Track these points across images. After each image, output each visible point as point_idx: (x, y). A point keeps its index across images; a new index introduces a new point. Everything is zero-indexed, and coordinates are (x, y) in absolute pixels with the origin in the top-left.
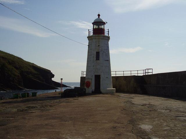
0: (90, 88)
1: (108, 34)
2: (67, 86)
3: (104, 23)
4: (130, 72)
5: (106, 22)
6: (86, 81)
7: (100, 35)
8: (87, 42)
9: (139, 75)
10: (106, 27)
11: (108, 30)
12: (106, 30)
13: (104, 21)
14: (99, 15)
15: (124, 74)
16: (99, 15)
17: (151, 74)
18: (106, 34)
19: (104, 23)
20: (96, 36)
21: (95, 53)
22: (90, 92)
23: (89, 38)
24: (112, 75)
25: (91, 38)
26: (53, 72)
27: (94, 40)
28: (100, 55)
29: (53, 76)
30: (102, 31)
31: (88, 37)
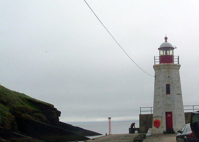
1: (178, 62)
2: (102, 135)
3: (173, 49)
6: (154, 119)
7: (170, 64)
8: (153, 72)
10: (176, 53)
12: (175, 57)
13: (173, 45)
14: (166, 38)
16: (166, 38)
17: (152, 108)
18: (176, 63)
19: (173, 49)
21: (165, 86)
22: (162, 132)
23: (155, 67)
24: (185, 111)
26: (57, 106)
27: (163, 70)
28: (165, 90)
29: (59, 113)
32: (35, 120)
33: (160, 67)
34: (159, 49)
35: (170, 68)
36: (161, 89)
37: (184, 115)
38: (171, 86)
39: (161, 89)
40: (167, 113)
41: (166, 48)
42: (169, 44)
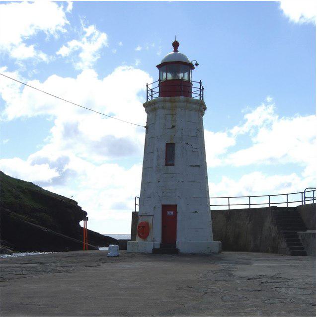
0: (149, 238)
3: (189, 67)
4: (226, 201)
5: (194, 63)
7: (176, 98)
9: (290, 205)
10: (195, 76)
11: (200, 83)
13: (191, 59)
14: (176, 45)
15: (229, 205)
16: (176, 45)
18: (195, 96)
19: (189, 67)
20: (165, 101)
21: (163, 147)
22: (149, 249)
25: (153, 107)
27: (161, 112)
28: (178, 151)
30: (184, 88)
31: (145, 105)
32: (30, 223)
33: (157, 106)
34: (159, 67)
35: (176, 108)
36: (156, 153)
37: (160, 209)
38: (176, 145)
39: (156, 153)
40: (165, 208)
41: (272, 130)
42: (182, 56)
